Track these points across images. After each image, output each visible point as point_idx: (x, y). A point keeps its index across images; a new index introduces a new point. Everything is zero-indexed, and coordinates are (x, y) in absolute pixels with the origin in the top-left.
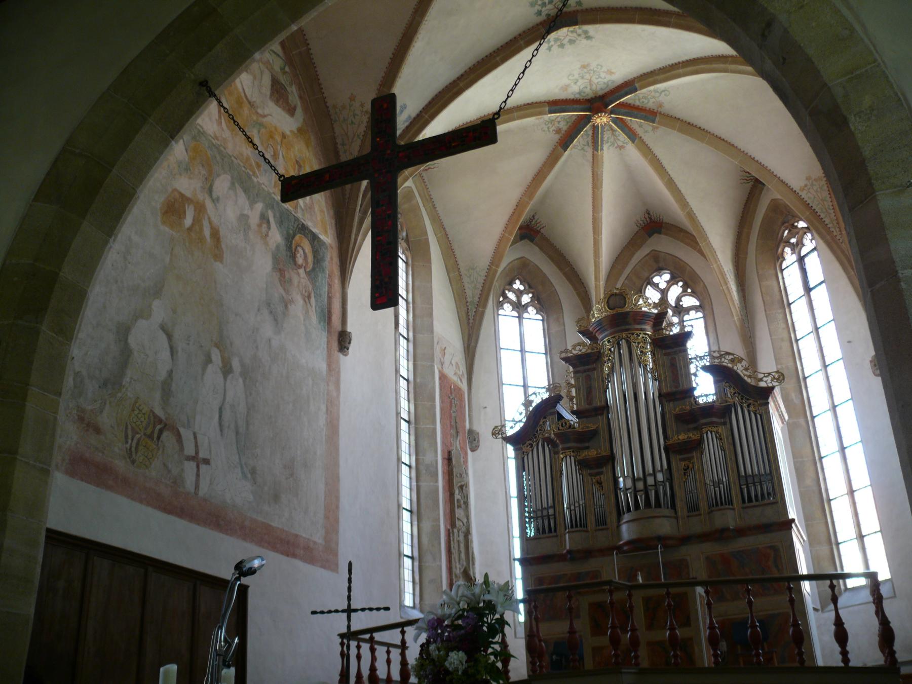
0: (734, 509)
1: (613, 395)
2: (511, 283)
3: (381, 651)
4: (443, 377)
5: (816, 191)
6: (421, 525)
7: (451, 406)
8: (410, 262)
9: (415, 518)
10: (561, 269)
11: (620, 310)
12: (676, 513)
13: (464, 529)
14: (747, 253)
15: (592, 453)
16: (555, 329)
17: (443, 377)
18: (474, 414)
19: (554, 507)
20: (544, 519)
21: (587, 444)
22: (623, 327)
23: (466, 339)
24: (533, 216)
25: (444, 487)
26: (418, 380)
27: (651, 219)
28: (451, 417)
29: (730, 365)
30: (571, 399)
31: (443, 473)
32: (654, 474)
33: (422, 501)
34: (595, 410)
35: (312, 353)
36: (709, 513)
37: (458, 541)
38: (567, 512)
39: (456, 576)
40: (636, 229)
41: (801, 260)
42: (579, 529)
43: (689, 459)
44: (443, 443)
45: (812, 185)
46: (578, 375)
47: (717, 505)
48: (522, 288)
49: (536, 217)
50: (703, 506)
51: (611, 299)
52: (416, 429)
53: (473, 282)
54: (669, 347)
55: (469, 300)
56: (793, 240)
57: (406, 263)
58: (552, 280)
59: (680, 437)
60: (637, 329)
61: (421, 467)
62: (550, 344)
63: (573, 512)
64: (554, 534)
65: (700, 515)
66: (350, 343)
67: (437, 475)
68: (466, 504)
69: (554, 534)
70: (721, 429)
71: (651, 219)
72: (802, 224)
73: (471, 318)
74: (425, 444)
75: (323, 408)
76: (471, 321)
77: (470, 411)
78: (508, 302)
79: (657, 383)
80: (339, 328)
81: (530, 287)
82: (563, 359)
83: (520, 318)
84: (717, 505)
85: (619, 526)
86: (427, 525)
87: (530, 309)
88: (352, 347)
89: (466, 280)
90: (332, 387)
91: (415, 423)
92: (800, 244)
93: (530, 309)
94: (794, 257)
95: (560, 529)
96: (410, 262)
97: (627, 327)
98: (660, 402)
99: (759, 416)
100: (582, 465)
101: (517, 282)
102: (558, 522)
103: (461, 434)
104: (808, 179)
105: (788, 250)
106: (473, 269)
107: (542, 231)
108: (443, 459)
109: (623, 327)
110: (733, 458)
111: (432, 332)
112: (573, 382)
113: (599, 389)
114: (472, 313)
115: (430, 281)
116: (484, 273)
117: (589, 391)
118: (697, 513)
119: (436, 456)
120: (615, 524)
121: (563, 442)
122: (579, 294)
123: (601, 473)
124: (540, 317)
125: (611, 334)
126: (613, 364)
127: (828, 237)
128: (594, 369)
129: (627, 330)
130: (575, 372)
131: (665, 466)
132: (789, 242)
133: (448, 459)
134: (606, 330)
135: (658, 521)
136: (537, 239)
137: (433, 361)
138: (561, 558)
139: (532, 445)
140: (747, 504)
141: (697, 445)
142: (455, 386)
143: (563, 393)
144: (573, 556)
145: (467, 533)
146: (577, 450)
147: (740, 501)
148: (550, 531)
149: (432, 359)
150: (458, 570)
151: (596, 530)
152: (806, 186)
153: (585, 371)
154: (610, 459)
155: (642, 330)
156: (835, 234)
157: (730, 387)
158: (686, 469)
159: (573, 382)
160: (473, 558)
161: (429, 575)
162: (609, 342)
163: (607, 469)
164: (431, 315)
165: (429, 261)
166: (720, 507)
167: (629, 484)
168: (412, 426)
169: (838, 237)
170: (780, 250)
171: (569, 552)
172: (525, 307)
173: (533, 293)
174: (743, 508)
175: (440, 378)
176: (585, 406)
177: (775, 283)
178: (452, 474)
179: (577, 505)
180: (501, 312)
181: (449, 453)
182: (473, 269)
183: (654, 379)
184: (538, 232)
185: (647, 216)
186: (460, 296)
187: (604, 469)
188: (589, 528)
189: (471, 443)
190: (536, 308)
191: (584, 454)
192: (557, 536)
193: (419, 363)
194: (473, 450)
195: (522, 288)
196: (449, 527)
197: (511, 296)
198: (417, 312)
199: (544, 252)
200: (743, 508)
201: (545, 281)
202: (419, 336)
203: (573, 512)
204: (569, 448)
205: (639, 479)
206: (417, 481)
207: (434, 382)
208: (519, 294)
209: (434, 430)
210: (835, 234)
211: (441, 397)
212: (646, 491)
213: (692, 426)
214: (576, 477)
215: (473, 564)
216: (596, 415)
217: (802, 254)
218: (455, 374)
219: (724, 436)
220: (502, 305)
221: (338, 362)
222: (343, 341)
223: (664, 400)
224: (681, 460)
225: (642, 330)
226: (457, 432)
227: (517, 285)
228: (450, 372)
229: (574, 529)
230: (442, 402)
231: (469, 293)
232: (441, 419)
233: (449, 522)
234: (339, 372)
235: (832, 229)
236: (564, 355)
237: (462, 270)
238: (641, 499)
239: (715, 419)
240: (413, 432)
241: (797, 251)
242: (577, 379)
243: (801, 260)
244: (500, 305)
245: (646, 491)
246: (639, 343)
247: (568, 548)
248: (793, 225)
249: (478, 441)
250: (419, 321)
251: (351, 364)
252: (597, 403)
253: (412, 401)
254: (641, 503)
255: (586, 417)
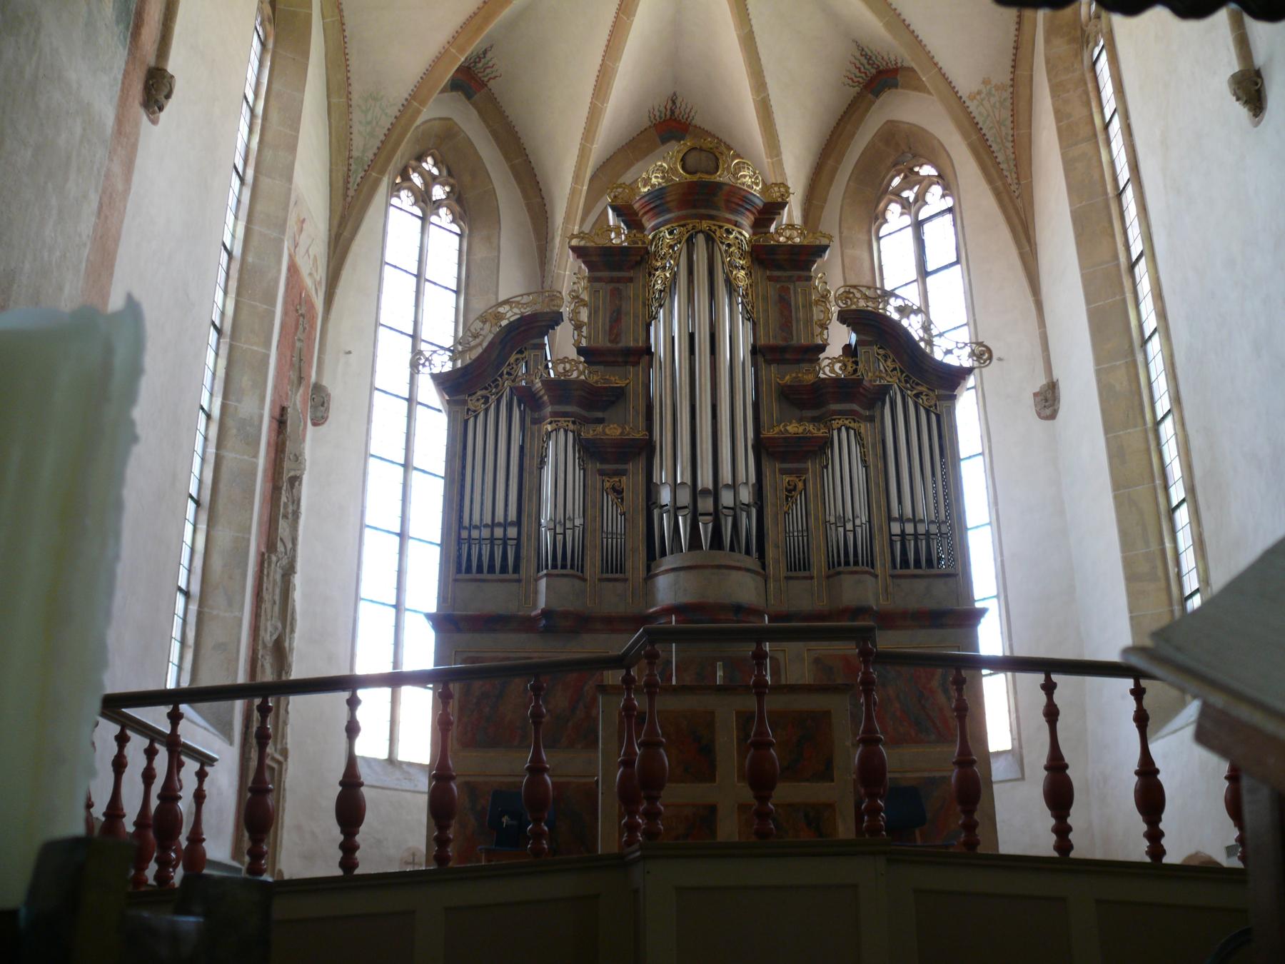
0: (876, 576)
1: (667, 331)
2: (420, 158)
3: (137, 744)
4: (293, 269)
5: (993, 106)
6: (212, 533)
7: (297, 328)
8: (270, 45)
9: (204, 517)
10: (507, 158)
11: (706, 178)
12: (764, 567)
13: (284, 562)
14: (825, 201)
15: (613, 431)
16: (481, 253)
17: (293, 269)
18: (328, 358)
19: (518, 523)
20: (479, 557)
21: (600, 415)
22: (703, 211)
23: (336, 222)
24: (485, 52)
25: (265, 471)
26: (250, 260)
27: (672, 112)
28: (293, 346)
29: (896, 316)
30: (578, 327)
31: (269, 444)
32: (734, 486)
33: (222, 487)
34: (621, 354)
35: (93, 78)
36: (828, 577)
37: (275, 580)
38: (547, 536)
39: (265, 646)
40: (647, 123)
41: (918, 226)
42: (568, 571)
43: (799, 473)
44: (275, 387)
45: (989, 94)
46: (597, 285)
47: (847, 563)
48: (435, 171)
49: (489, 55)
50: (819, 562)
51: (694, 153)
52: (231, 349)
53: (369, 123)
54: (780, 267)
55: (355, 154)
56: (909, 194)
57: (263, 44)
58: (492, 175)
59: (789, 428)
60: (729, 221)
61: (230, 423)
62: (468, 276)
63: (560, 538)
64: (510, 576)
65: (812, 578)
66: (168, 96)
67: (259, 444)
68: (296, 514)
69: (510, 576)
70: (864, 428)
71: (672, 112)
72: (927, 170)
73: (353, 187)
74: (244, 380)
75: (94, 199)
76: (351, 193)
77: (319, 358)
78: (410, 189)
79: (749, 325)
80: (151, 61)
81: (450, 174)
82: (574, 249)
83: (424, 219)
84: (847, 563)
85: (650, 576)
86: (224, 536)
87: (443, 211)
88: (171, 106)
89: (356, 116)
90: (117, 168)
91: (234, 336)
92: (921, 199)
93: (443, 211)
94: (907, 220)
95: (528, 568)
96: (270, 45)
97: (714, 213)
98: (755, 364)
99: (933, 417)
100: (589, 451)
101: (430, 160)
102: (524, 552)
103: (304, 383)
104: (986, 82)
105: (895, 208)
106: (375, 99)
107: (492, 84)
108: (272, 417)
109: (703, 211)
110: (882, 484)
111: (290, 179)
112: (585, 296)
113: (636, 316)
114: (356, 178)
115: (302, 89)
116: (393, 111)
117: (616, 318)
118: (807, 574)
119: (262, 408)
120: (642, 573)
121: (556, 400)
122: (530, 208)
123: (623, 473)
124: (456, 229)
125: (677, 219)
126: (675, 276)
127: (999, 183)
128: (631, 280)
129: (712, 218)
130: (592, 280)
131: (753, 479)
132: (898, 195)
133: (281, 421)
134: (669, 211)
135: (735, 575)
136: (477, 97)
137: (283, 232)
138: (526, 624)
139: (486, 399)
140: (899, 571)
141: (819, 448)
142: (308, 296)
143: (566, 310)
144: (553, 623)
145: (289, 571)
146: (581, 421)
147: (889, 565)
148: (504, 569)
149: (282, 227)
150: (268, 637)
151: (601, 580)
152: (979, 93)
153: (612, 280)
154: (645, 449)
155: (736, 224)
156: (1009, 181)
157: (886, 357)
158: (791, 490)
159: (585, 296)
160: (293, 619)
161: (216, 633)
162: (671, 233)
163: (635, 470)
164: (292, 148)
165: (306, 54)
166: (852, 568)
167: (684, 497)
168: (225, 341)
169: (1013, 187)
170: (882, 205)
171: (546, 613)
172: (438, 204)
173: (452, 187)
174: (893, 576)
175: (289, 269)
176: (602, 342)
177: (866, 256)
178: (283, 451)
179: (569, 525)
180: (394, 201)
181: (283, 410)
182: (375, 99)
183: (749, 317)
184: (483, 85)
185: (670, 104)
186: (340, 141)
187: (630, 466)
188: (588, 574)
189: (315, 408)
190: (452, 212)
191: (589, 433)
192: (519, 581)
193: (256, 228)
194: (315, 424)
195: (435, 171)
196: (263, 550)
197: (416, 179)
198: (269, 136)
199: (485, 121)
200: (893, 576)
201: (478, 169)
202: (265, 182)
203: (560, 538)
204: (565, 415)
205: (705, 492)
206: (219, 446)
207: (279, 271)
208: (430, 180)
209: (268, 356)
210: (1009, 181)
211: (285, 303)
212: (716, 515)
213: (809, 413)
214: (575, 476)
215: (292, 631)
216: (626, 363)
217: (921, 217)
218: (310, 274)
219: (869, 440)
220: (399, 190)
221: (137, 125)
222: (155, 88)
223: (760, 359)
224: (783, 472)
225: (736, 224)
226: (300, 379)
227: (429, 165)
228: (305, 267)
229: (559, 571)
230: (285, 313)
231: (358, 142)
232: (279, 342)
233: (264, 539)
234: (134, 147)
235: (1006, 173)
236: (574, 242)
237: (355, 96)
238: (705, 530)
239: (855, 407)
240: (224, 352)
241: (913, 210)
242: (594, 293)
243: (918, 226)
244: (395, 190)
245: (716, 515)
246: (729, 245)
247: (542, 604)
248: (911, 170)
249: (327, 409)
250: (268, 154)
251: (162, 138)
252: (630, 340)
253: (232, 294)
254: (705, 541)
255: (607, 364)
